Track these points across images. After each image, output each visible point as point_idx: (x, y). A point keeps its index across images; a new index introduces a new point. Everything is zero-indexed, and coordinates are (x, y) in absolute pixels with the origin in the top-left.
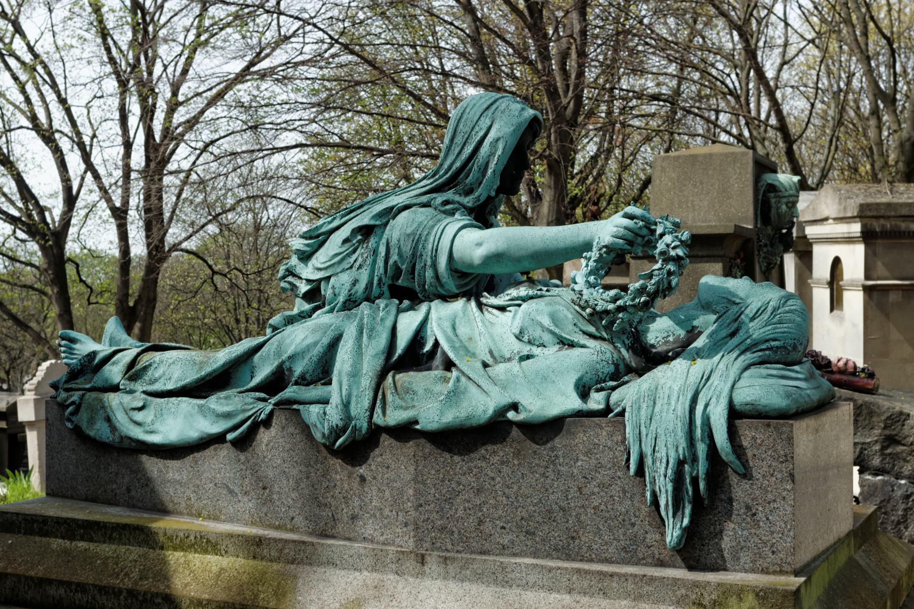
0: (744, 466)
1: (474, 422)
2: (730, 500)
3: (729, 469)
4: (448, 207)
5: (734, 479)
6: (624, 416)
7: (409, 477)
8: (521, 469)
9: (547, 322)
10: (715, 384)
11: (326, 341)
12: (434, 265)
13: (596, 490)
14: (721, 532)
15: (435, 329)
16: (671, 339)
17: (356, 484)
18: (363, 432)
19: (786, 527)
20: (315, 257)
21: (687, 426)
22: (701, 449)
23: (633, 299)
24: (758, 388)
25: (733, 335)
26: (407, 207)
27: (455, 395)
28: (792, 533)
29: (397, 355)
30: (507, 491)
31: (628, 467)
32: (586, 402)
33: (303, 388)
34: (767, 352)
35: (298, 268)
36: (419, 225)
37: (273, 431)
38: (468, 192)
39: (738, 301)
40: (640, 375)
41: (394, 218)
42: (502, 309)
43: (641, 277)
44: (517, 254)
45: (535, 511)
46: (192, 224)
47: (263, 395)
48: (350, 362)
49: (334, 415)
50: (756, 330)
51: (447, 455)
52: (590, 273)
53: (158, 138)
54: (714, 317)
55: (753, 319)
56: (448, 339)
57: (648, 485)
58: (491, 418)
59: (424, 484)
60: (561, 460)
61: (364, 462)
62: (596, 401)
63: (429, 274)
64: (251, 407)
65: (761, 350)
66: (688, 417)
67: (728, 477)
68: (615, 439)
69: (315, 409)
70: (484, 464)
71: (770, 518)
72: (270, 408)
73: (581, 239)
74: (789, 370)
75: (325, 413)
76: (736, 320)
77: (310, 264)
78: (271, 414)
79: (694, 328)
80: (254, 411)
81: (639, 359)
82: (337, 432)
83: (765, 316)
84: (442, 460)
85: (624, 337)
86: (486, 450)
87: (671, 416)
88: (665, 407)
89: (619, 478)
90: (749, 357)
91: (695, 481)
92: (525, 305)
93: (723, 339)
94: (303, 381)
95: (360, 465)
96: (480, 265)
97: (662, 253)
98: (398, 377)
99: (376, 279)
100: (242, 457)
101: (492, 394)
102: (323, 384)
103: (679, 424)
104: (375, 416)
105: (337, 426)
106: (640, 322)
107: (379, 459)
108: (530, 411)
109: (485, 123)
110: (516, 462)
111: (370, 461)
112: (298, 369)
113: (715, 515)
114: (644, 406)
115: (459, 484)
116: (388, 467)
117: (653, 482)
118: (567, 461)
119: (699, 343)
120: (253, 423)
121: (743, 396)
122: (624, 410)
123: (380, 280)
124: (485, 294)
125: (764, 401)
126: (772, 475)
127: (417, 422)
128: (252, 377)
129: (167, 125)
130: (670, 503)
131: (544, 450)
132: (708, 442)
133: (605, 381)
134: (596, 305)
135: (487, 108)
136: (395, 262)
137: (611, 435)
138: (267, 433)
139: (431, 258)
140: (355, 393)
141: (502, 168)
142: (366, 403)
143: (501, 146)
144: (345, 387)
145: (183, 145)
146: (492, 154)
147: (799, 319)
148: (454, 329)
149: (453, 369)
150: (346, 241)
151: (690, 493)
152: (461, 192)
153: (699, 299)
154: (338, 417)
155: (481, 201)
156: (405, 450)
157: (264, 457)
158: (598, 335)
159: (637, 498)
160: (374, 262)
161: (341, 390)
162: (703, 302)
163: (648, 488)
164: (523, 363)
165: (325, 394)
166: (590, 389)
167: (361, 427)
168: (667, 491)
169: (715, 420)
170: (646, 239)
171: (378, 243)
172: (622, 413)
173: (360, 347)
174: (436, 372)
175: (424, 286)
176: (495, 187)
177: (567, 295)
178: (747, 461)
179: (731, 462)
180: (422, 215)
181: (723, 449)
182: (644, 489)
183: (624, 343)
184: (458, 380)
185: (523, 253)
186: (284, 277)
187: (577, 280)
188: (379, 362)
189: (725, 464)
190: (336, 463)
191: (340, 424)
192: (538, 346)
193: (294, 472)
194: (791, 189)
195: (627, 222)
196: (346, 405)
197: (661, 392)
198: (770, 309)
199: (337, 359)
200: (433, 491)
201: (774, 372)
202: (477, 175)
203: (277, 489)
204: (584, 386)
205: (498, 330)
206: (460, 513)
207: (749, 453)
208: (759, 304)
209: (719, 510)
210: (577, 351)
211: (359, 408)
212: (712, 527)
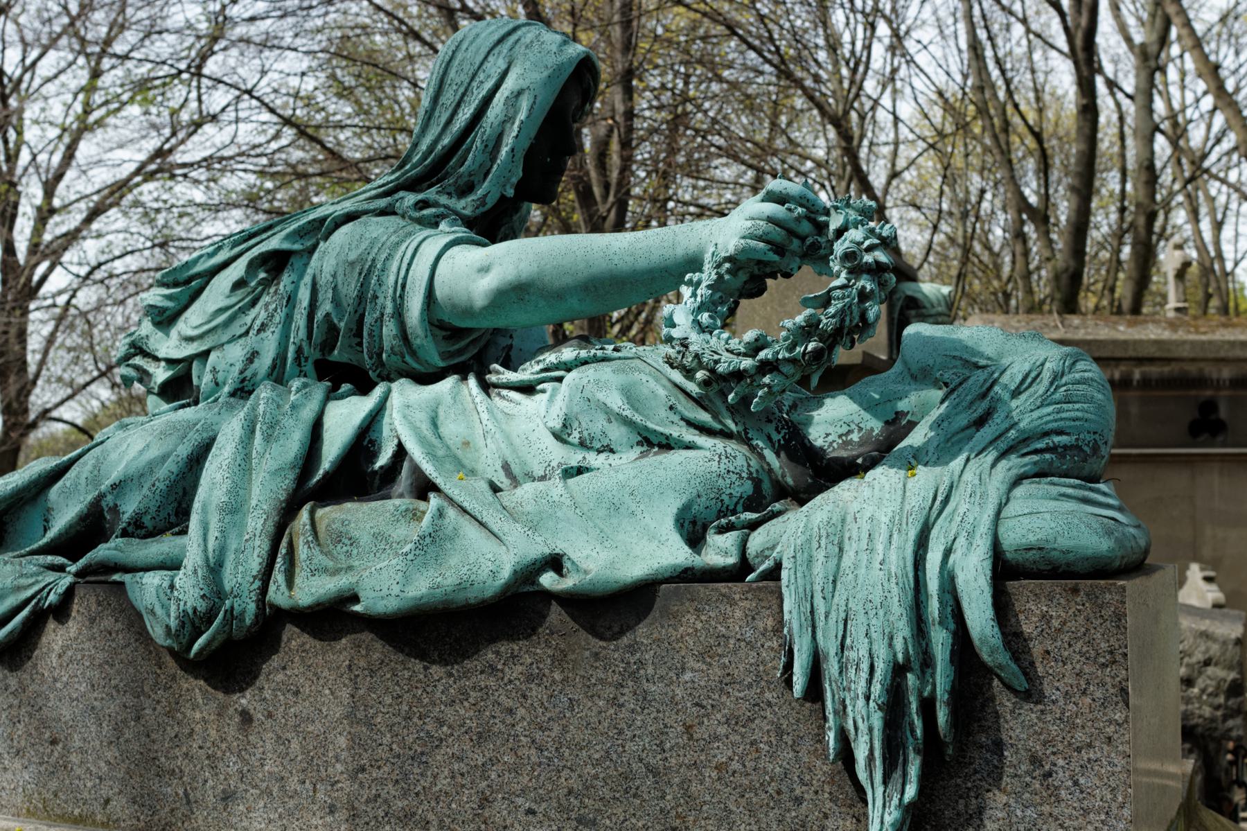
0: (1025, 674)
1: (472, 595)
2: (998, 747)
3: (996, 682)
5: (1005, 702)
6: (779, 579)
7: (338, 712)
8: (568, 690)
9: (616, 402)
10: (961, 510)
11: (184, 450)
12: (399, 314)
13: (722, 730)
14: (980, 811)
15: (396, 423)
16: (855, 437)
17: (232, 731)
18: (248, 622)
19: (1114, 799)
20: (183, 318)
21: (910, 594)
22: (940, 640)
23: (791, 348)
24: (1048, 516)
25: (980, 422)
26: (350, 217)
27: (433, 543)
28: (1126, 812)
29: (321, 472)
30: (538, 735)
31: (789, 683)
32: (699, 554)
33: (135, 541)
34: (1048, 456)
35: (152, 340)
36: (372, 244)
37: (73, 627)
38: (465, 189)
39: (983, 362)
40: (802, 503)
41: (326, 238)
42: (528, 389)
43: (806, 303)
44: (557, 284)
45: (596, 777)
46: (71, 384)
47: (59, 560)
48: (227, 484)
49: (189, 589)
50: (1025, 413)
51: (417, 665)
52: (701, 308)
53: (21, 256)
54: (940, 394)
55: (1016, 393)
56: (422, 441)
57: (831, 717)
58: (507, 587)
59: (370, 725)
60: (650, 671)
61: (250, 684)
62: (720, 550)
63: (389, 330)
64: (31, 581)
65: (1036, 452)
66: (911, 575)
67: (993, 699)
68: (761, 625)
69: (153, 580)
70: (492, 682)
71: (1082, 781)
72: (66, 581)
73: (680, 252)
74: (1091, 490)
75: (172, 587)
76: (984, 396)
77: (174, 332)
78: (69, 593)
79: (899, 415)
80: (36, 588)
81: (800, 469)
82: (194, 623)
83: (1040, 388)
84: (407, 674)
85: (770, 429)
86: (497, 653)
87: (877, 574)
88: (864, 557)
89: (769, 704)
90: (1014, 464)
91: (927, 707)
92: (570, 377)
93: (963, 430)
94: (139, 529)
95: (242, 690)
96: (485, 308)
98: (320, 512)
99: (291, 350)
100: (13, 682)
101: (509, 539)
102: (173, 534)
103: (895, 590)
104: (272, 588)
105: (195, 610)
106: (794, 407)
107: (280, 677)
108: (586, 572)
109: (496, 65)
110: (557, 676)
111: (262, 680)
112: (130, 507)
113: (967, 777)
114: (820, 556)
115: (441, 723)
116: (297, 693)
117: (842, 711)
118: (662, 671)
119: (916, 438)
120: (33, 613)
121: (1016, 534)
122: (778, 566)
123: (299, 351)
124: (496, 366)
125: (1064, 542)
126: (1084, 693)
127: (355, 599)
128: (45, 530)
129: (35, 240)
130: (878, 753)
131: (614, 651)
132: (952, 626)
133: (734, 512)
134: (716, 362)
135: (501, 41)
136: (328, 315)
137: (752, 617)
138: (61, 631)
139: (394, 300)
140: (233, 545)
141: (527, 145)
142: (255, 564)
143: (525, 104)
144: (213, 533)
145: (59, 269)
146: (508, 119)
147: (1100, 396)
148: (434, 424)
149: (432, 495)
150: (239, 285)
151: (919, 732)
152: (452, 189)
153: (905, 363)
154: (197, 593)
155: (488, 206)
156: (330, 656)
157: (55, 680)
158: (718, 426)
159: (807, 745)
160: (289, 318)
161: (205, 540)
162: (914, 368)
163: (831, 722)
164: (571, 481)
165: (176, 551)
166: (705, 528)
167: (243, 612)
168: (871, 729)
169: (966, 582)
170: (809, 241)
171: (296, 284)
172: (774, 574)
173: (247, 457)
174: (397, 502)
175: (380, 355)
176: (514, 180)
177: (656, 354)
178: (1032, 664)
179: (1000, 667)
180: (378, 228)
181: (983, 641)
182: (822, 727)
183: (769, 438)
184: (441, 514)
185: (568, 280)
186: (126, 358)
187: (676, 320)
188: (285, 484)
189: (987, 672)
190: (195, 687)
191: (202, 606)
192: (599, 452)
193: (113, 708)
194: (939, 304)
195: (771, 208)
196: (214, 569)
197: (854, 527)
198: (1046, 376)
199: (202, 481)
200: (387, 739)
201: (1070, 491)
202: (480, 159)
203: (78, 744)
204: (694, 523)
205: (519, 428)
206: (443, 783)
207: (1037, 649)
208: (1027, 367)
209: (976, 766)
210: (676, 457)
211: (240, 575)
212: (961, 801)
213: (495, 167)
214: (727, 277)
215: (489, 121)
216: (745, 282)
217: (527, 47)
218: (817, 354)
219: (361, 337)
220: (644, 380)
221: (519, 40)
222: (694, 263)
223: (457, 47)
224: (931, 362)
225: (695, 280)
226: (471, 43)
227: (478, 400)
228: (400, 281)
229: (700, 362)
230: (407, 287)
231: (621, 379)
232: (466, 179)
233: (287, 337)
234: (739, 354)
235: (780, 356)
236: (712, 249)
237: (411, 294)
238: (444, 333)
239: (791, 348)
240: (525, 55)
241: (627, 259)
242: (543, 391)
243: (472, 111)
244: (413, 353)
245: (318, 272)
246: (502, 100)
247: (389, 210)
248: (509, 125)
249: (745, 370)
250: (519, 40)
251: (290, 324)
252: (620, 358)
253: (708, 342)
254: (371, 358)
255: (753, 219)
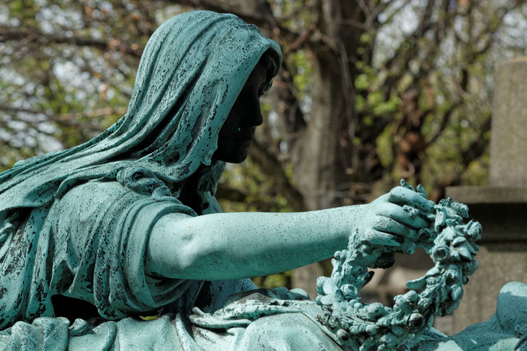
4: (142, 182)
12: (122, 268)
23: (400, 317)
36: (99, 208)
38: (172, 159)
42: (221, 331)
44: (242, 253)
52: (343, 281)
63: (115, 279)
73: (333, 232)
92: (252, 326)
96: (188, 267)
97: (440, 253)
123: (40, 288)
134: (351, 325)
135: (200, 36)
136: (64, 262)
139: (118, 257)
141: (221, 124)
143: (219, 92)
146: (207, 104)
152: (161, 158)
155: (191, 173)
160: (31, 261)
170: (421, 232)
175: (106, 298)
176: (211, 152)
177: (311, 309)
185: (250, 250)
187: (326, 290)
213: (196, 141)
214: (364, 255)
215: (191, 105)
216: (378, 258)
217: (221, 42)
218: (417, 322)
219: (92, 281)
220: (304, 332)
221: (214, 35)
222: (341, 242)
223: (165, 39)
224: (513, 317)
225: (342, 256)
226: (176, 37)
227: (183, 340)
228: (123, 242)
229: (340, 324)
230: (128, 247)
231: (286, 331)
232: (172, 151)
233: (30, 277)
234: (365, 320)
235: (392, 323)
236: (354, 233)
237: (131, 253)
238: (156, 281)
239: (400, 317)
240: (219, 49)
241: (294, 235)
242: (232, 334)
243: (176, 95)
244: (133, 297)
245: (54, 226)
246: (201, 89)
247: (111, 177)
248: (206, 109)
249: (369, 332)
250: (214, 35)
251: (32, 267)
252: (288, 312)
253: (345, 310)
254: (99, 300)
255: (381, 215)
